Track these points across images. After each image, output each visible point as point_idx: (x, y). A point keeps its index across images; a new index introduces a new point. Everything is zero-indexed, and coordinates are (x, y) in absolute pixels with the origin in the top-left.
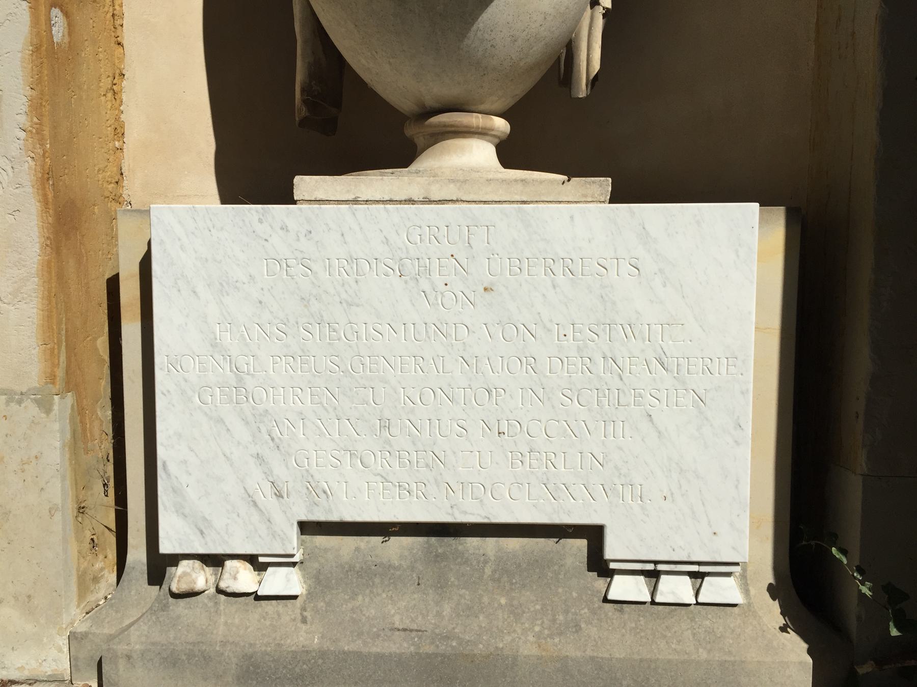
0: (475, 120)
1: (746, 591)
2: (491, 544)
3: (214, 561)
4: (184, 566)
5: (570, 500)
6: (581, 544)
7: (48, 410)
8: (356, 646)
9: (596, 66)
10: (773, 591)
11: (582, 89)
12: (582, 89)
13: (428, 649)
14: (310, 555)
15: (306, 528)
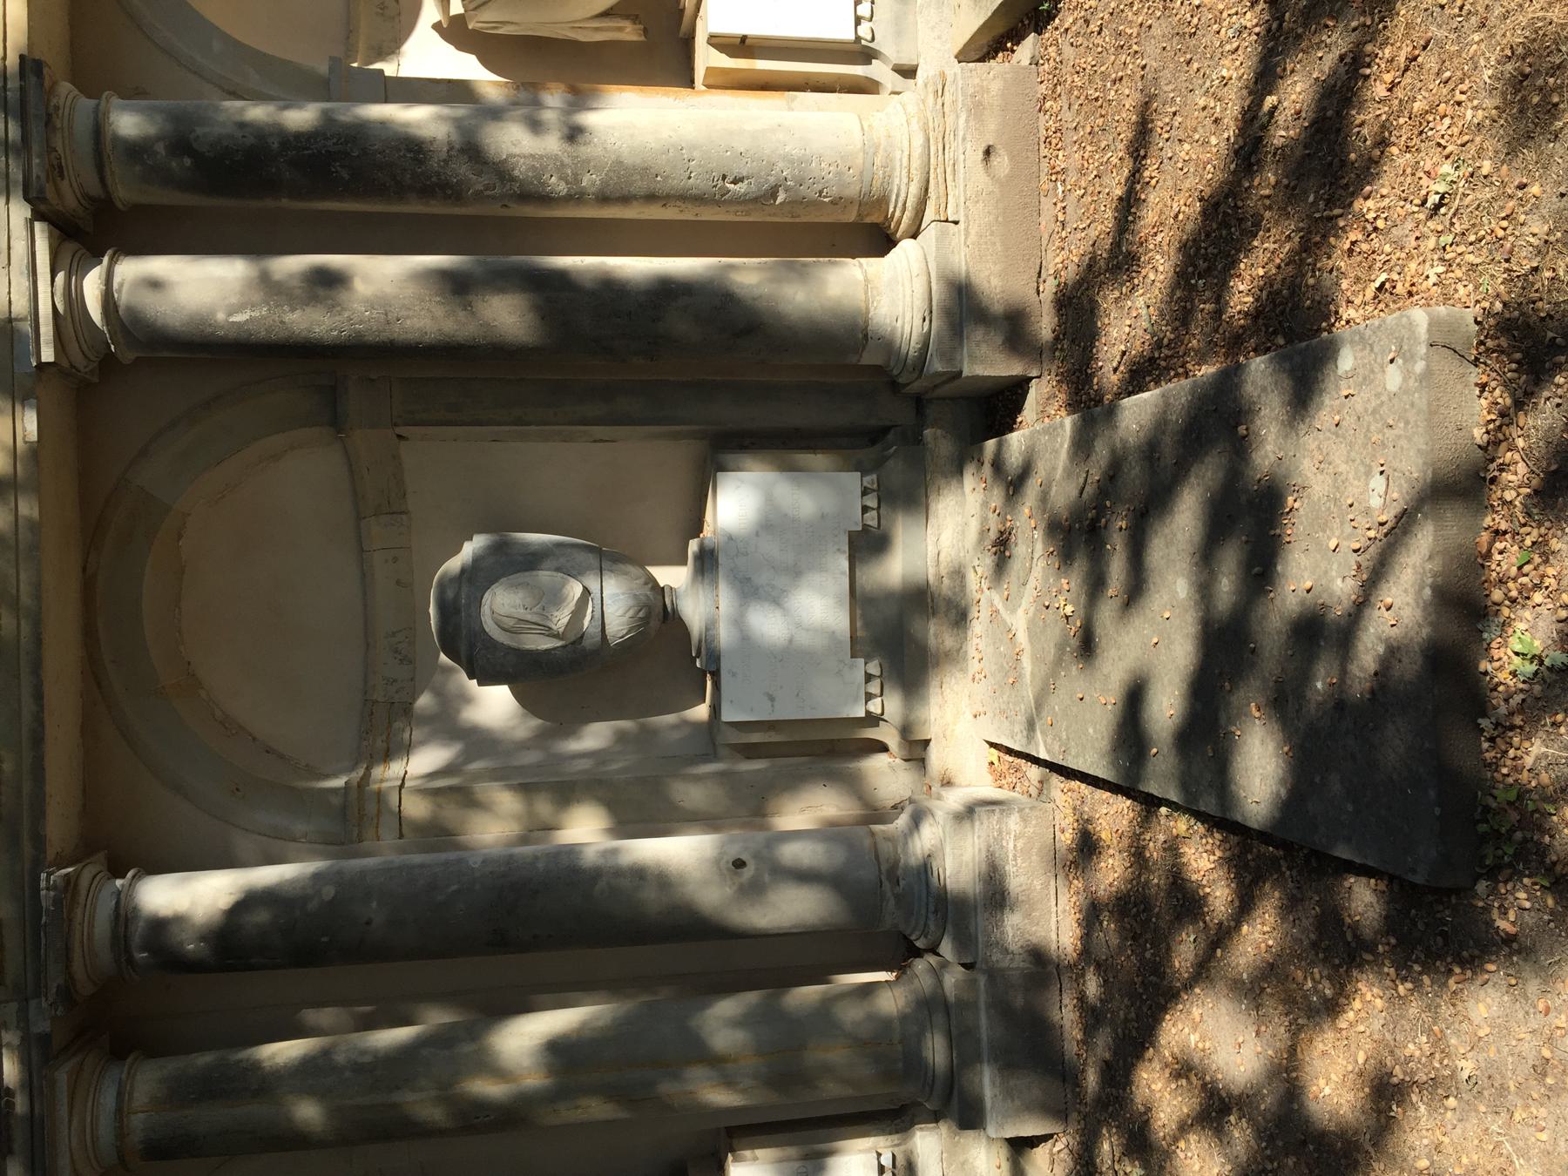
3: (858, 21)
4: (860, 33)
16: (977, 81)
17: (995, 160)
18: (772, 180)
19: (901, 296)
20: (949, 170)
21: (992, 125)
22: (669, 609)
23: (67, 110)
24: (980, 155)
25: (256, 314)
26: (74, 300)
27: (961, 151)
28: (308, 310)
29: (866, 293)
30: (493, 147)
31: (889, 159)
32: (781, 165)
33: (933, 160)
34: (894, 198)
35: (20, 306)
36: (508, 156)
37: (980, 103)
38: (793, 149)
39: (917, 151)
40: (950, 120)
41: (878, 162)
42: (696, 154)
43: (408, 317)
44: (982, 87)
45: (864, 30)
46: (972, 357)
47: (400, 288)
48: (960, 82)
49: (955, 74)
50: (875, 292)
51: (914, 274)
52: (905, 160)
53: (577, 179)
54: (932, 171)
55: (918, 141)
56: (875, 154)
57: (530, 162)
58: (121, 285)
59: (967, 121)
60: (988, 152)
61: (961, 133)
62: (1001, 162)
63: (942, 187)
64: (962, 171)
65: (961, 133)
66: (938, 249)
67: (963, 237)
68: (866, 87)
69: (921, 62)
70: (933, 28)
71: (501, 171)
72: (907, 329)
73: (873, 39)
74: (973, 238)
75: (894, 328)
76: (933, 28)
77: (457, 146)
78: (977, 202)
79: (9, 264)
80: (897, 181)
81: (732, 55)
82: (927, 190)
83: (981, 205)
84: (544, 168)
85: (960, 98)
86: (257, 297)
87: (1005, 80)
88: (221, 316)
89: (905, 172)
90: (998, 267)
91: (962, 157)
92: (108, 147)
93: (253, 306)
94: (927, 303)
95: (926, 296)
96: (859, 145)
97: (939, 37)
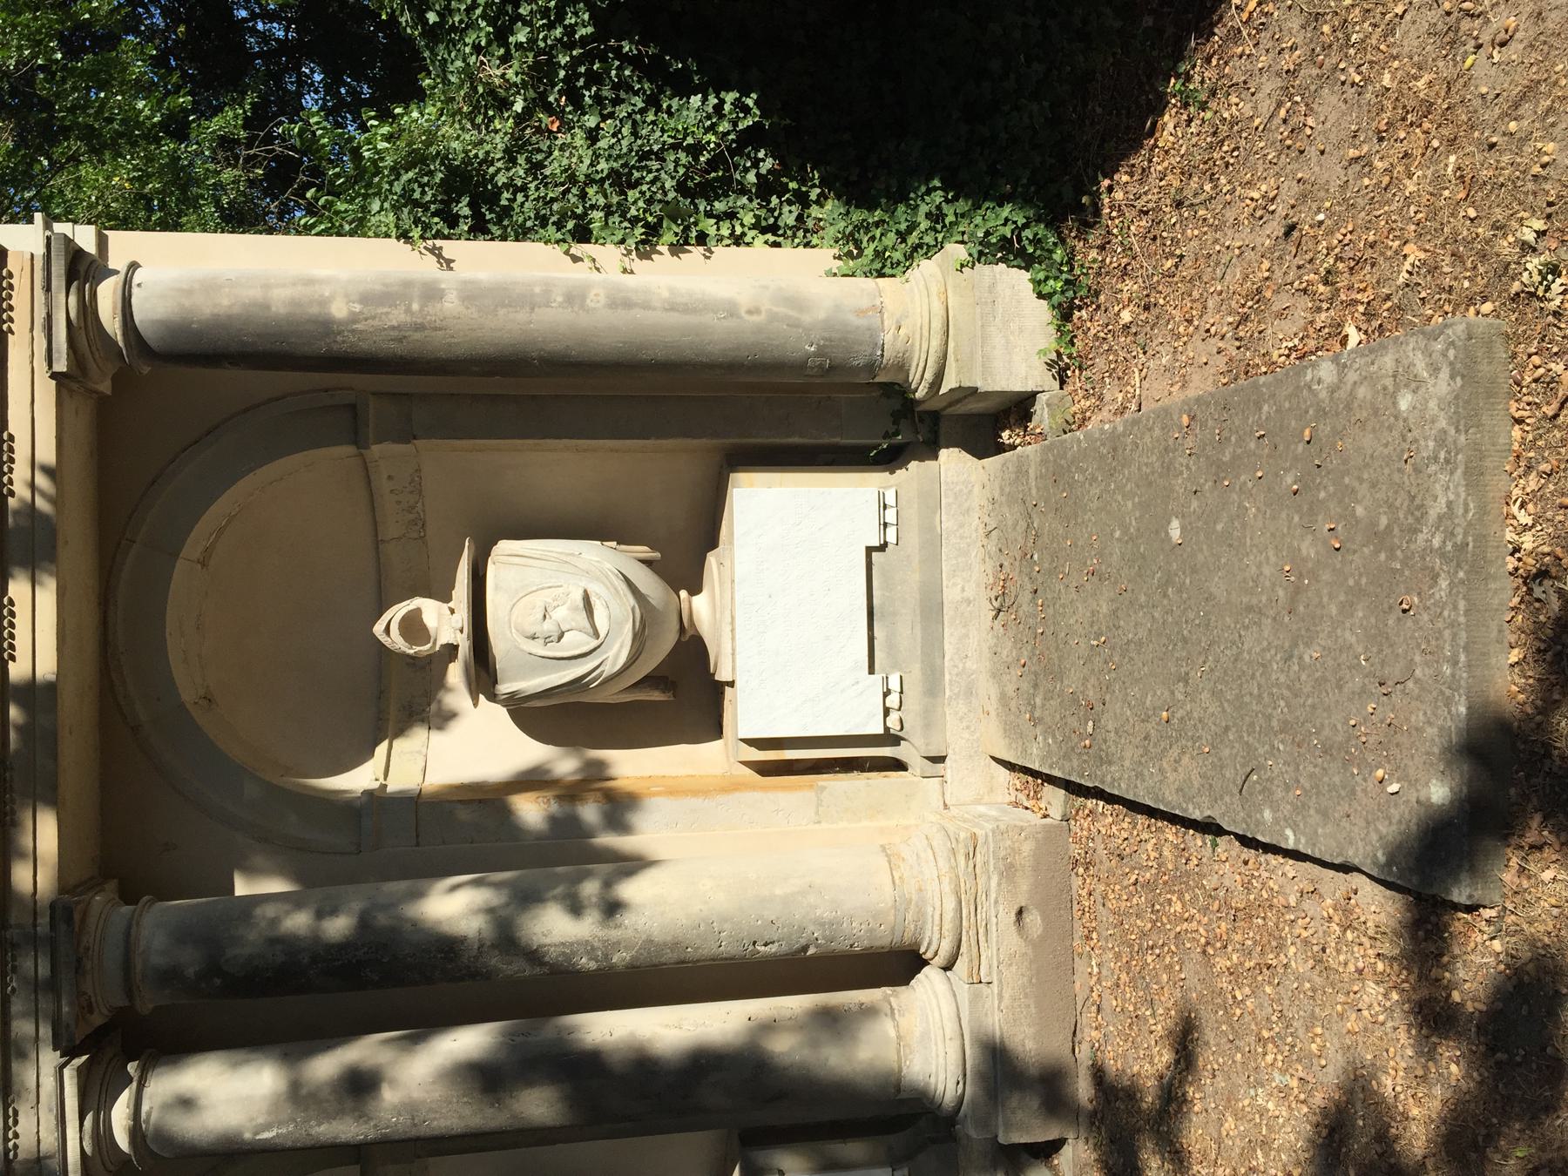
0: (685, 606)
1: (891, 486)
2: (875, 593)
3: (887, 711)
4: (889, 724)
5: (954, 316)
6: (874, 554)
7: (824, 788)
8: (919, 648)
9: (47, 453)
10: (892, 472)
11: (657, 555)
12: (657, 555)
13: (919, 618)
14: (883, 670)
15: (871, 671)
16: (1009, 843)
17: (1028, 918)
18: (803, 942)
19: (934, 1054)
20: (981, 931)
21: (1024, 885)
22: (686, 624)
23: (96, 948)
24: (1013, 917)
25: (283, 1131)
26: (103, 1136)
27: (993, 914)
28: (334, 1123)
29: (899, 1052)
30: (523, 940)
31: (921, 914)
32: (811, 928)
33: (965, 923)
34: (914, 364)
35: (49, 1140)
36: (539, 946)
37: (1012, 865)
38: (825, 913)
39: (949, 915)
40: (981, 881)
41: (909, 917)
42: (727, 926)
43: (435, 1119)
44: (1013, 849)
45: (893, 722)
46: (1008, 1126)
47: (427, 1092)
48: (992, 846)
49: (987, 836)
50: (908, 1051)
51: (948, 1037)
52: (937, 918)
53: (606, 957)
54: (964, 933)
55: (950, 904)
56: (906, 910)
57: (561, 949)
58: (149, 1114)
59: (999, 884)
60: (1020, 912)
61: (993, 896)
62: (1033, 919)
63: (975, 950)
64: (995, 934)
65: (993, 896)
66: (971, 1013)
67: (996, 1002)
68: (898, 765)
69: (950, 752)
70: (961, 719)
71: (534, 956)
72: (942, 1077)
73: (902, 729)
74: (1006, 1001)
75: (928, 1084)
76: (961, 719)
77: (488, 943)
78: (1011, 965)
79: (38, 1102)
80: (928, 933)
81: (760, 748)
82: (959, 947)
83: (1014, 968)
84: (574, 953)
85: (992, 862)
86: (287, 1110)
87: (1037, 840)
88: (247, 1136)
89: (936, 928)
90: (1032, 1030)
91: (994, 920)
92: (139, 967)
93: (280, 1124)
94: (961, 1068)
95: (960, 1063)
96: (890, 903)
97: (968, 727)
